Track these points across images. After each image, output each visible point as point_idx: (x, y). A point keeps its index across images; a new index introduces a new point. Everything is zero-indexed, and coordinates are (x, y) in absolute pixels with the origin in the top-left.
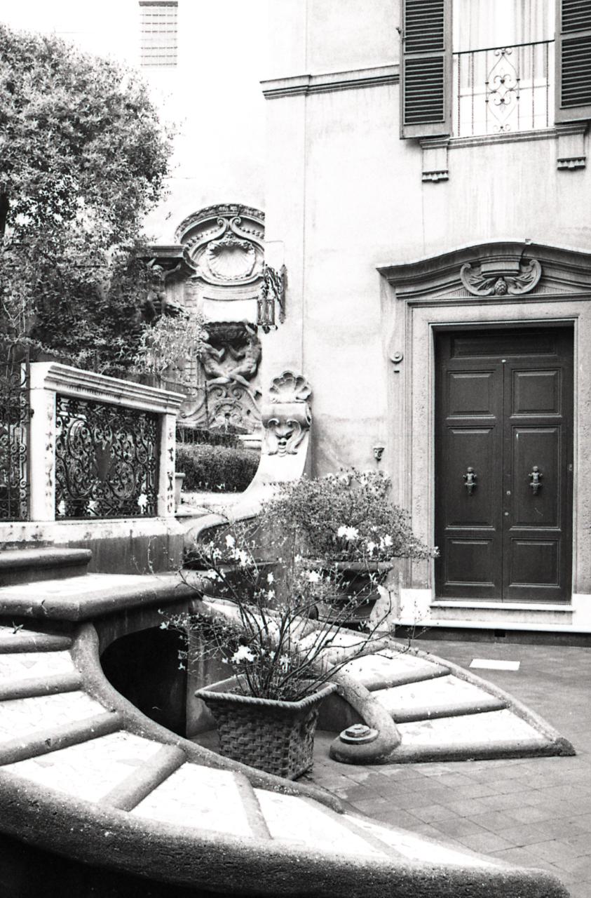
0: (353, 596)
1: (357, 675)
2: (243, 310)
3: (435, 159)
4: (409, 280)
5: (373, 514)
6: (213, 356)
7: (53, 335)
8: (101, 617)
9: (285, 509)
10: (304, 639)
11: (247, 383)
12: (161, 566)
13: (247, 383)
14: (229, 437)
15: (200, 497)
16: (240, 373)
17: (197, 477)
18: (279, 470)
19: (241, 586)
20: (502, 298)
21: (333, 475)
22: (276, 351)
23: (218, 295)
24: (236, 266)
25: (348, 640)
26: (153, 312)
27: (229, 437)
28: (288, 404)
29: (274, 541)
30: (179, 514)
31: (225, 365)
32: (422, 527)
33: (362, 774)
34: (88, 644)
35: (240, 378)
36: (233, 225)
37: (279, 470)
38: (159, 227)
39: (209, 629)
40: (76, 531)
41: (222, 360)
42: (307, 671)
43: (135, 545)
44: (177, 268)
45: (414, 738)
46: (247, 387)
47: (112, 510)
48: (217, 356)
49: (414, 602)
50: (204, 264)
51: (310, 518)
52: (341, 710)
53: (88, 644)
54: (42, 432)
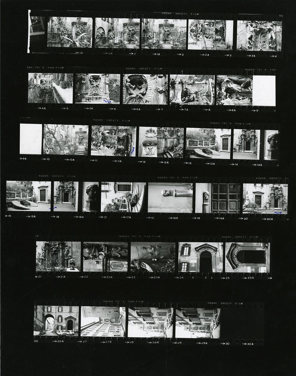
0: (131, 195)
1: (134, 195)
2: (117, 200)
3: (110, 191)
4: (116, 192)
5: (127, 194)
6: (131, 87)
7: (118, 209)
8: (131, 207)
9: (126, 198)
10: (133, 197)
11: (143, 97)
12: (129, 204)
13: (143, 97)
14: (123, 201)
15: (126, 202)
16: (140, 93)
17: (125, 202)
18: (125, 198)
19: (130, 200)
20: (116, 188)
21: (125, 196)
22: (119, 199)
23: (116, 201)
24: (115, 200)
25: (133, 195)
26: (117, 204)
27: (123, 201)
28: (121, 198)
29: (128, 199)
30: (127, 203)
31: (135, 91)
32: (127, 192)
33: (139, 195)
34: (133, 208)
35: (140, 95)
36: (113, 200)
37: (125, 198)
38: (113, 204)
39: (132, 202)
40: (127, 208)
41: (134, 89)
42: (134, 197)
43: (128, 205)
44: (115, 203)
45: (137, 192)
46: (143, 98)
47: (126, 206)
48: (133, 88)
49: (131, 192)
50: (115, 202)
51: (127, 197)
52: (136, 196)
53: (133, 208)
54: (123, 210)
